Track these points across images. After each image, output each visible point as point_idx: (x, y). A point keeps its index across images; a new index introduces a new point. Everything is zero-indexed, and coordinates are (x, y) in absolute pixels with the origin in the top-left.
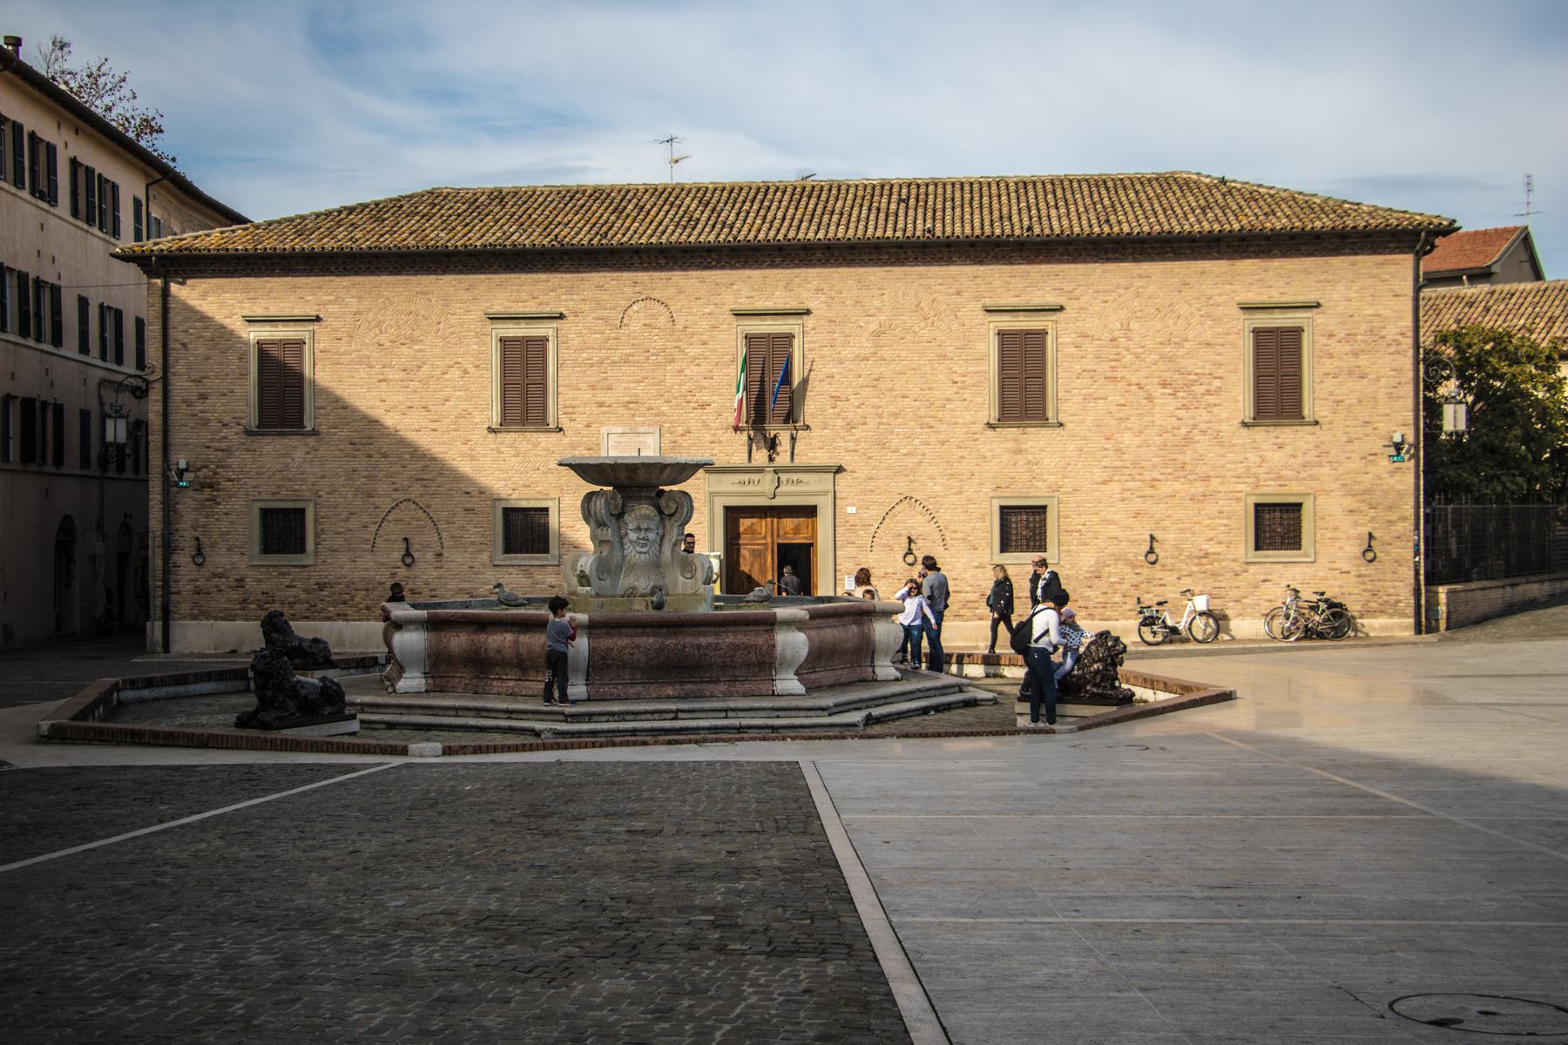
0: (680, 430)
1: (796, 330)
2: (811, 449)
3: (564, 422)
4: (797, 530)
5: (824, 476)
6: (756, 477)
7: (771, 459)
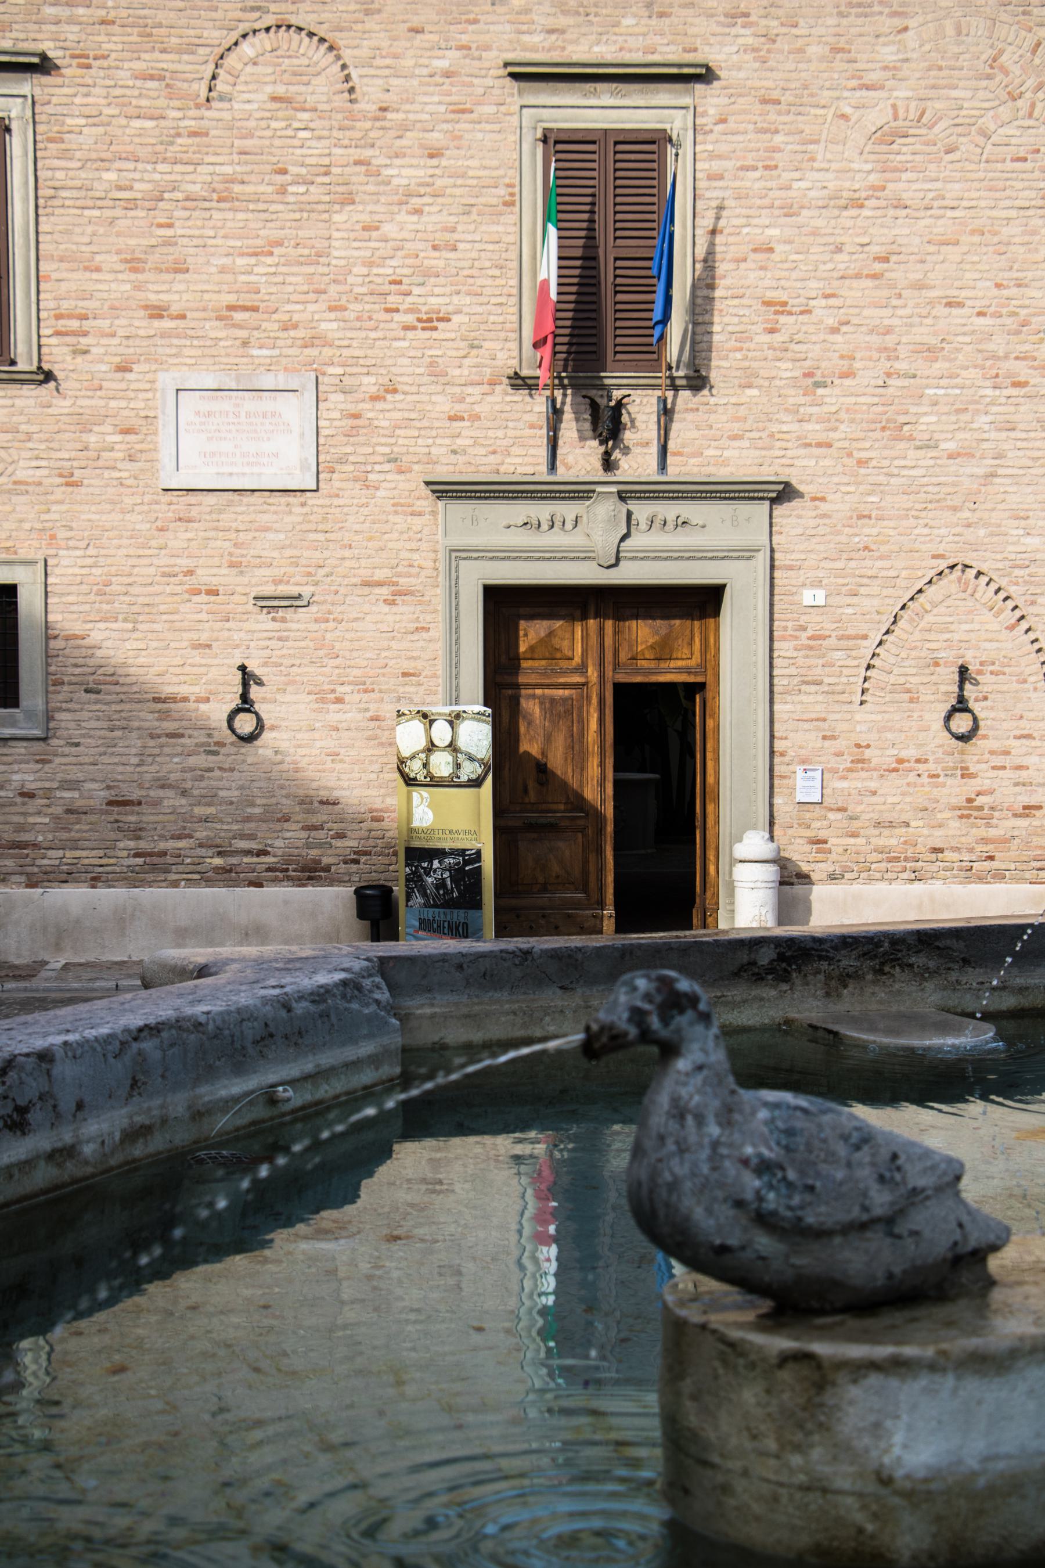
0: (370, 383)
1: (676, 123)
2: (711, 438)
3: (57, 355)
4: (663, 651)
5: (745, 509)
6: (568, 510)
7: (608, 464)
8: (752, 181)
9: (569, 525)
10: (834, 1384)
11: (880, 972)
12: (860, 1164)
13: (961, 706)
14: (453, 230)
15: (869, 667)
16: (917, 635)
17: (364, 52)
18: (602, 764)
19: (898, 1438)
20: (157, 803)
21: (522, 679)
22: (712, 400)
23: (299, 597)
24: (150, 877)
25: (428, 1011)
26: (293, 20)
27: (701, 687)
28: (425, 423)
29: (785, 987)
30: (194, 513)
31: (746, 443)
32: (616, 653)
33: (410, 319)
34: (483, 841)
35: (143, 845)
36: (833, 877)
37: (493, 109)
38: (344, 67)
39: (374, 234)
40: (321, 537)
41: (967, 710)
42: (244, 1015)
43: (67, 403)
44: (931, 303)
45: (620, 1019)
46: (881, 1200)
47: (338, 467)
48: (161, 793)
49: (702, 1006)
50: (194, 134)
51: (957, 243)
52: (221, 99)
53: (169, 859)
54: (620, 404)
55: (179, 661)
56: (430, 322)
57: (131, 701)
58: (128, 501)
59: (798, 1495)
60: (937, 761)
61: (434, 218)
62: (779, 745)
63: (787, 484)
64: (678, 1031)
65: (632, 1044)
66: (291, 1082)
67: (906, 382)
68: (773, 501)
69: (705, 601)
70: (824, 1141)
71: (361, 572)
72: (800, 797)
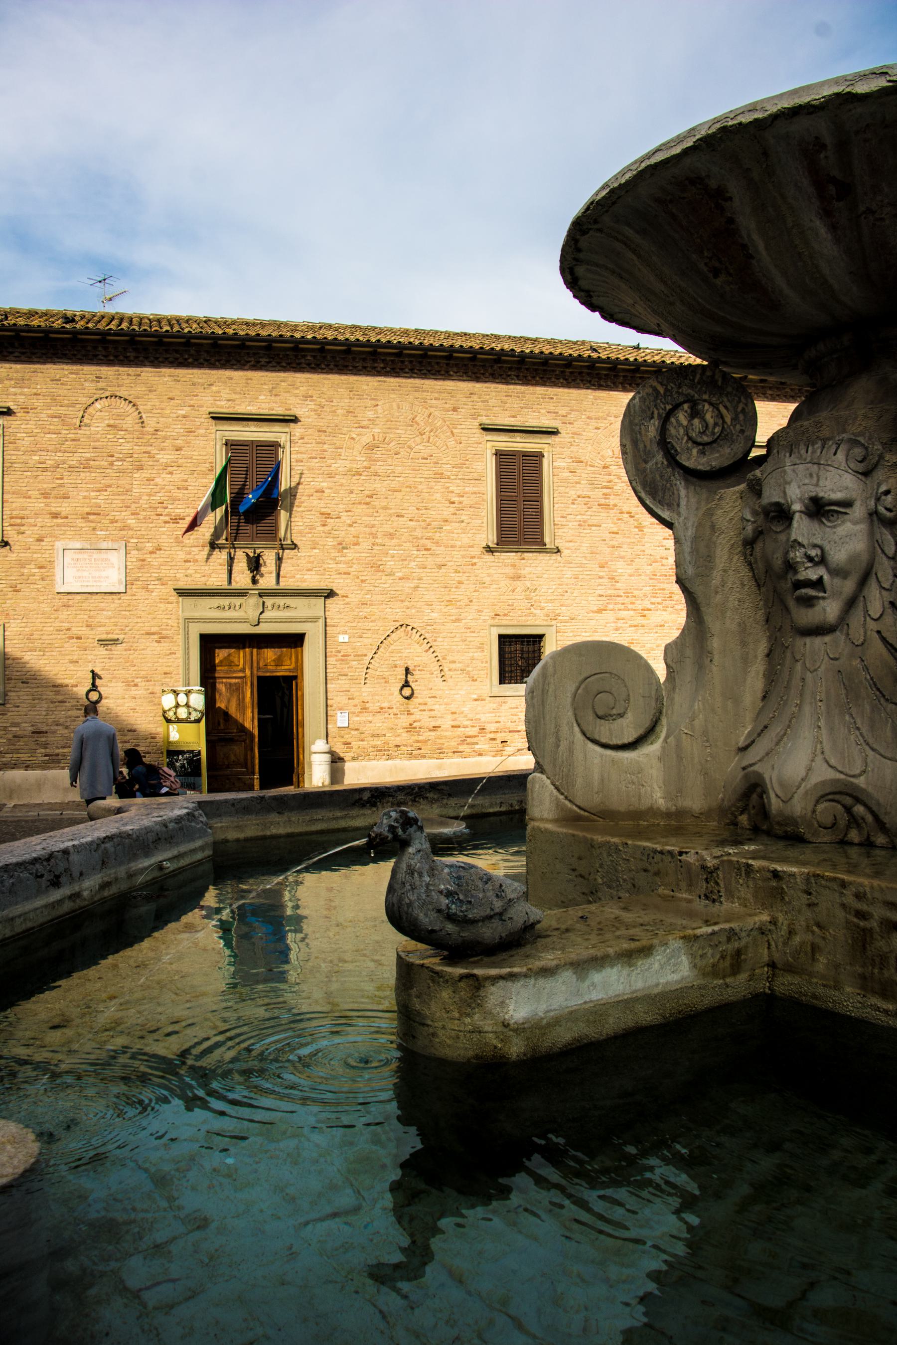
0: (149, 546)
1: (283, 439)
2: (299, 571)
4: (279, 662)
5: (313, 600)
6: (237, 601)
7: (254, 581)
8: (315, 463)
9: (237, 608)
10: (484, 986)
11: (414, 801)
12: (488, 890)
13: (407, 684)
14: (186, 481)
15: (367, 668)
16: (388, 654)
17: (149, 407)
18: (253, 712)
19: (511, 1007)
20: (54, 732)
21: (217, 675)
22: (299, 554)
23: (118, 640)
24: (51, 765)
25: (219, 825)
26: (118, 394)
27: (295, 677)
28: (174, 563)
29: (374, 809)
30: (71, 603)
31: (314, 573)
32: (258, 663)
33: (167, 518)
34: (201, 746)
35: (48, 751)
36: (354, 759)
37: (204, 431)
38: (139, 413)
39: (152, 483)
40: (127, 613)
41: (409, 686)
42: (148, 830)
43: (15, 555)
44: (390, 515)
45: (385, 830)
46: (498, 905)
47: (135, 583)
48: (56, 728)
49: (419, 824)
50: (73, 440)
51: (400, 491)
52: (86, 426)
53: (60, 757)
54: (259, 556)
55: (64, 669)
57: (42, 687)
58: (41, 598)
59: (468, 1035)
60: (397, 708)
61: (178, 476)
62: (329, 702)
63: (331, 590)
64: (410, 835)
65: (389, 842)
66: (168, 860)
67: (381, 548)
68: (326, 597)
69: (296, 640)
70: (473, 881)
71: (145, 628)
72: (339, 725)
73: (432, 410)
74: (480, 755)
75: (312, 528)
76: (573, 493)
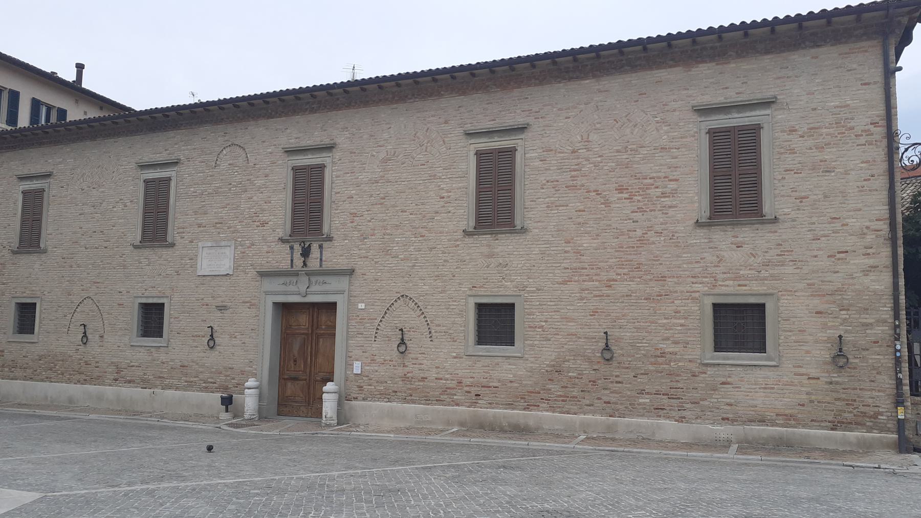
2: (333, 256)
3: (529, 224)
13: (402, 342)
35: (188, 379)
41: (404, 343)
56: (264, 224)
72: (355, 372)
73: (429, 125)
74: (457, 405)
75: (344, 224)
76: (542, 179)
